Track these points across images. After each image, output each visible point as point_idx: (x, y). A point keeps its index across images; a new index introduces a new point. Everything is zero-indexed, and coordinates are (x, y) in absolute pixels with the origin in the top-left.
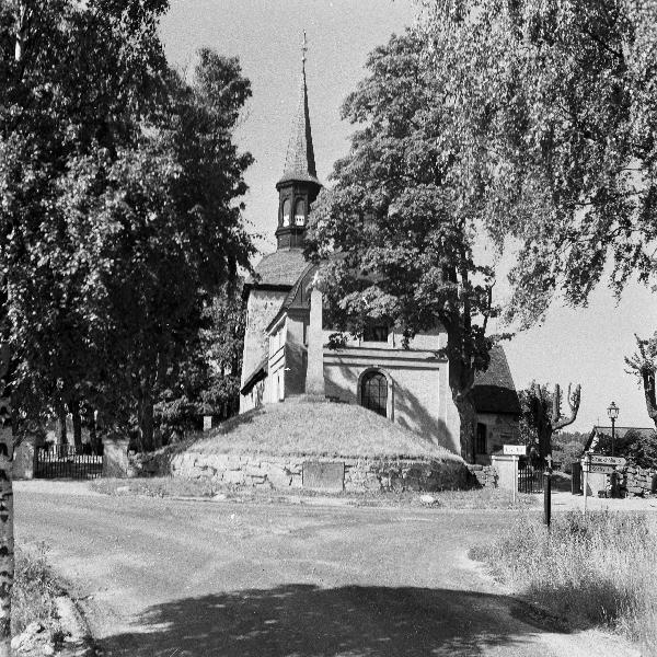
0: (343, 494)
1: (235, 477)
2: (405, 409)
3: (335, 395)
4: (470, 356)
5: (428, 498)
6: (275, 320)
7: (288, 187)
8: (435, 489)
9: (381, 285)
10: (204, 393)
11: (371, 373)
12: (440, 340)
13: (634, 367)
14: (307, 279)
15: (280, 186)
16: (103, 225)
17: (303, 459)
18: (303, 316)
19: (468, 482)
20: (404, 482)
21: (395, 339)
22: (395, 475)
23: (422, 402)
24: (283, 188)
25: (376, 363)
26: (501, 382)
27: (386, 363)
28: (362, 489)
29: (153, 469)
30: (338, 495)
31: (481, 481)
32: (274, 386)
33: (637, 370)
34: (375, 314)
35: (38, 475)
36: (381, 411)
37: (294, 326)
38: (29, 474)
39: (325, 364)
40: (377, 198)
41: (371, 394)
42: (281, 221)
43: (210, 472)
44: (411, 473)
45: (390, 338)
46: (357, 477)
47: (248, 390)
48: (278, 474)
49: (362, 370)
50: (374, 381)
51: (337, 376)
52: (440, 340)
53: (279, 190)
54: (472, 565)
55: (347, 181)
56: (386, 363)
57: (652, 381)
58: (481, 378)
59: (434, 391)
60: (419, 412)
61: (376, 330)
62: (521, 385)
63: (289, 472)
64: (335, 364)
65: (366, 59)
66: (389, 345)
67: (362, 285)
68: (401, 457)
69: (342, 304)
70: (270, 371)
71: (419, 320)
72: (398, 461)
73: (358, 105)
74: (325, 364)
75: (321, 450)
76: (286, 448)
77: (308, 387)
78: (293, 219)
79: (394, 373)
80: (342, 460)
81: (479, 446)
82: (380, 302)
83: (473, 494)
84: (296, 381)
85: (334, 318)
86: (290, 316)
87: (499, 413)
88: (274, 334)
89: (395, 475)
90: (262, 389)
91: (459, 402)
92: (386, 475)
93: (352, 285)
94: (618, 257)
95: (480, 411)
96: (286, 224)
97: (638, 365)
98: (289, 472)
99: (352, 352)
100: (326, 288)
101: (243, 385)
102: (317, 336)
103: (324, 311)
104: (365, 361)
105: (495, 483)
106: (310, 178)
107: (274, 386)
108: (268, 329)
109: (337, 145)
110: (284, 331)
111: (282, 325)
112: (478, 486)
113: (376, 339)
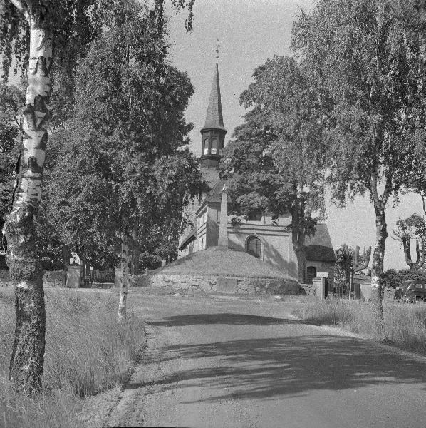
0: (237, 294)
1: (184, 286)
2: (273, 257)
3: (233, 247)
4: (303, 227)
5: (278, 297)
6: (200, 210)
7: (208, 131)
8: (283, 294)
9: (258, 191)
10: (157, 250)
11: (252, 237)
12: (286, 220)
13: (398, 236)
14: (219, 187)
15: (203, 132)
16: (167, 182)
17: (217, 277)
18: (217, 206)
19: (301, 291)
20: (267, 289)
21: (267, 220)
22: (262, 286)
23: (279, 251)
24: (205, 132)
25: (255, 232)
26: (323, 243)
27: (261, 232)
28: (246, 292)
29: (138, 284)
30: (233, 295)
31: (307, 292)
32: (200, 244)
33: (399, 238)
34: (255, 206)
35: (81, 286)
36: (257, 256)
37: (210, 211)
38: (77, 284)
39: (228, 232)
40: (256, 147)
41: (251, 248)
42: (203, 152)
43: (170, 284)
44: (271, 285)
45: (263, 218)
46: (243, 287)
47: (183, 248)
48: (205, 285)
49: (247, 236)
50: (254, 241)
51: (234, 238)
52: (286, 220)
53: (202, 133)
54: (292, 316)
55: (241, 138)
56: (261, 232)
57: (409, 244)
58: (309, 241)
59: (284, 246)
60: (278, 257)
61: (255, 214)
62: (336, 246)
63: (210, 284)
64: (234, 233)
65: (253, 72)
66: (261, 223)
67: (249, 191)
68: (265, 277)
69: (238, 200)
70: (198, 236)
71: (277, 210)
72: (264, 279)
73: (245, 97)
74: (228, 232)
75: (226, 272)
76: (210, 272)
77: (219, 243)
78: (210, 151)
79: (265, 237)
80: (236, 278)
81: (310, 274)
82: (259, 200)
83: (302, 297)
84: (212, 240)
85: (233, 208)
86: (209, 206)
87: (317, 256)
88: (200, 216)
89: (262, 286)
90: (193, 246)
91: (297, 252)
92: (258, 286)
93: (242, 191)
94: (351, 188)
95: (310, 259)
96: (206, 153)
97: (400, 235)
98: (210, 284)
99: (242, 226)
100: (230, 193)
101: (180, 245)
102: (224, 218)
103: (229, 204)
104: (249, 231)
105: (315, 294)
106: (220, 127)
107: (200, 244)
108: (197, 213)
109: (235, 117)
110: (206, 214)
111: (205, 211)
112: (305, 294)
113: (256, 220)
